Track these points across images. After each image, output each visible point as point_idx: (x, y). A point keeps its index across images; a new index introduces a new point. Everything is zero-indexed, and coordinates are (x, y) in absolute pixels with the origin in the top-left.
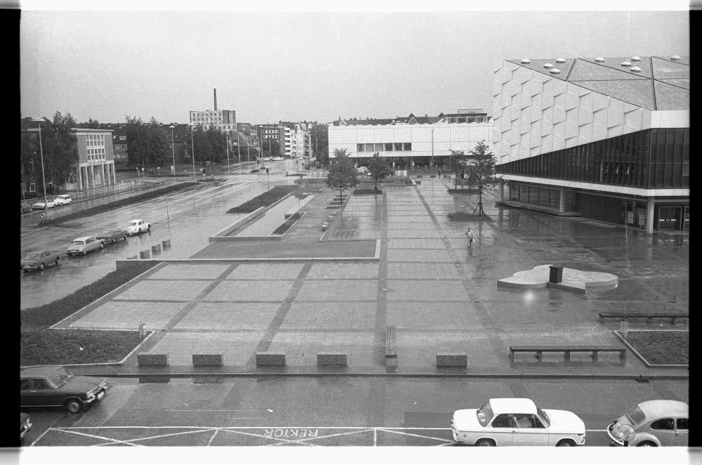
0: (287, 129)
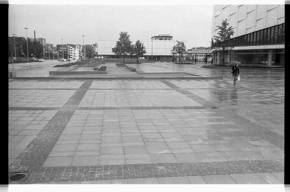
0: (71, 47)
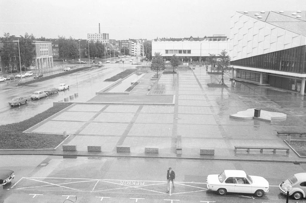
0: (132, 42)
